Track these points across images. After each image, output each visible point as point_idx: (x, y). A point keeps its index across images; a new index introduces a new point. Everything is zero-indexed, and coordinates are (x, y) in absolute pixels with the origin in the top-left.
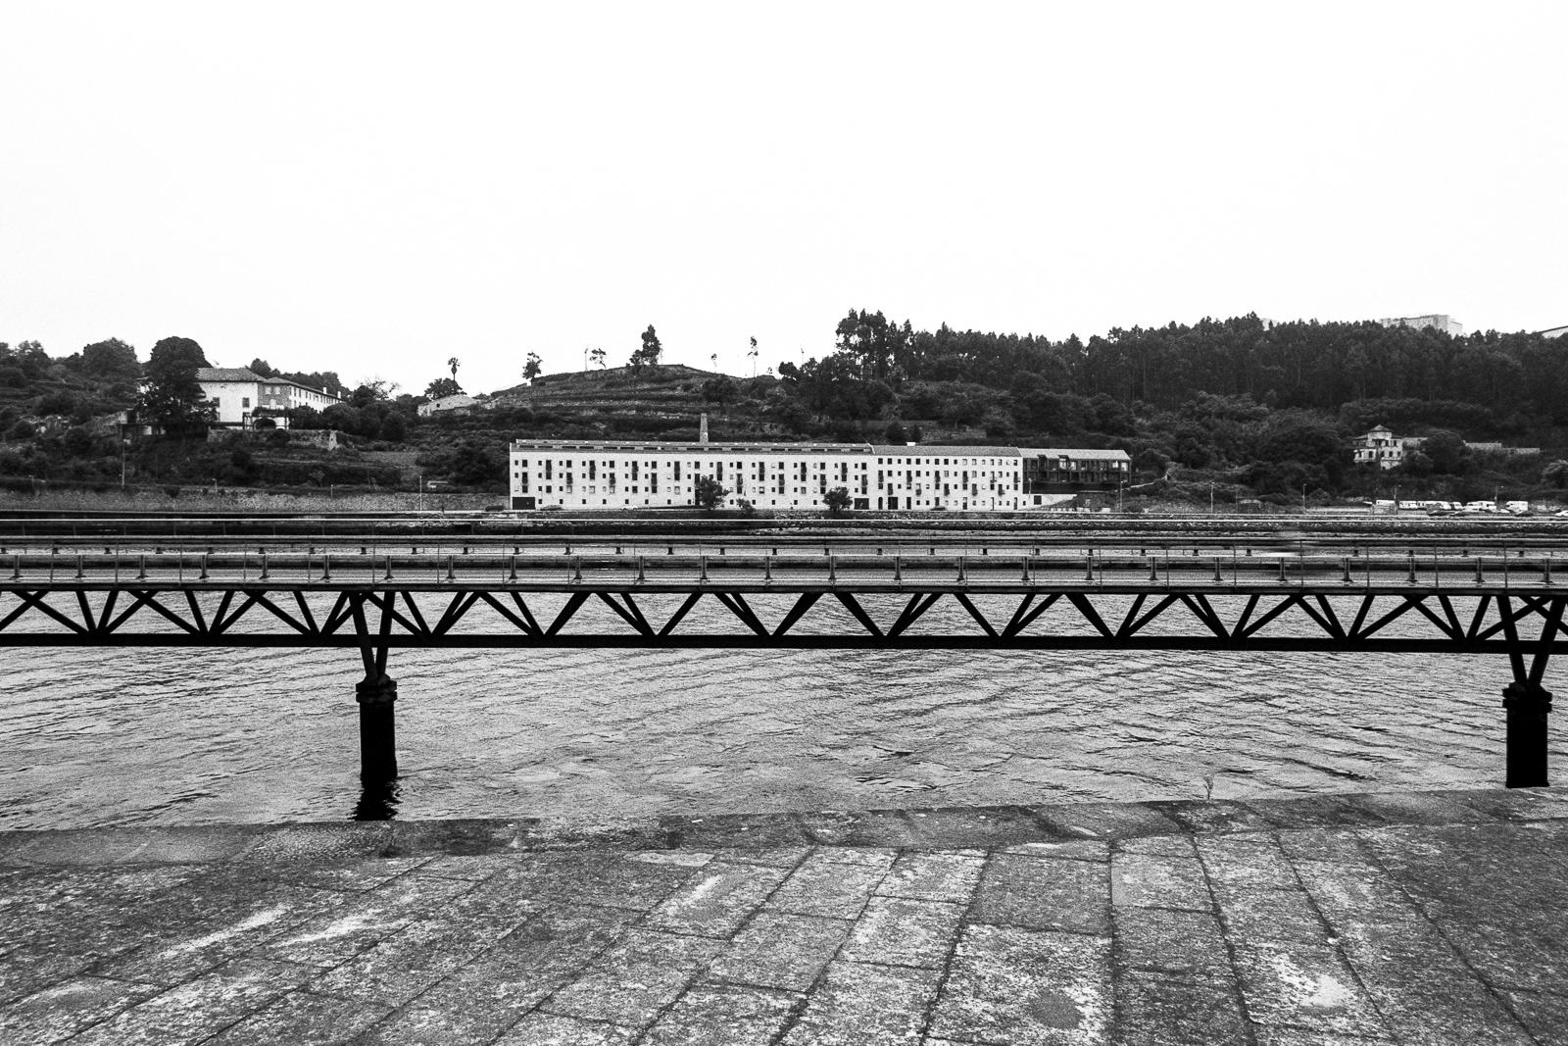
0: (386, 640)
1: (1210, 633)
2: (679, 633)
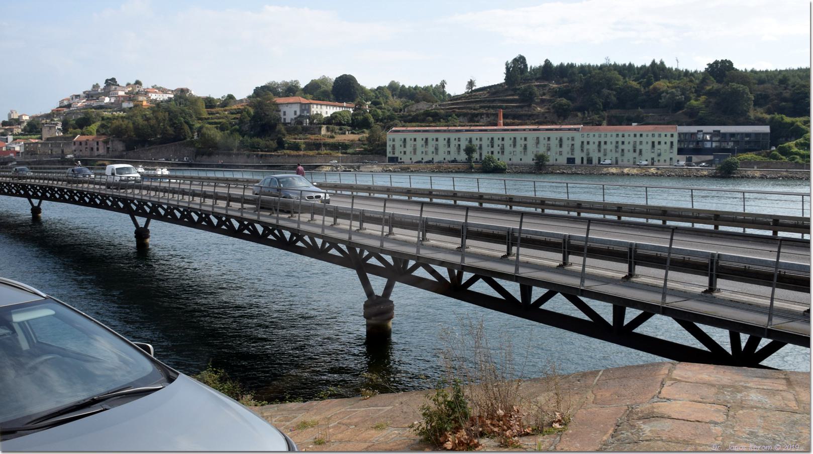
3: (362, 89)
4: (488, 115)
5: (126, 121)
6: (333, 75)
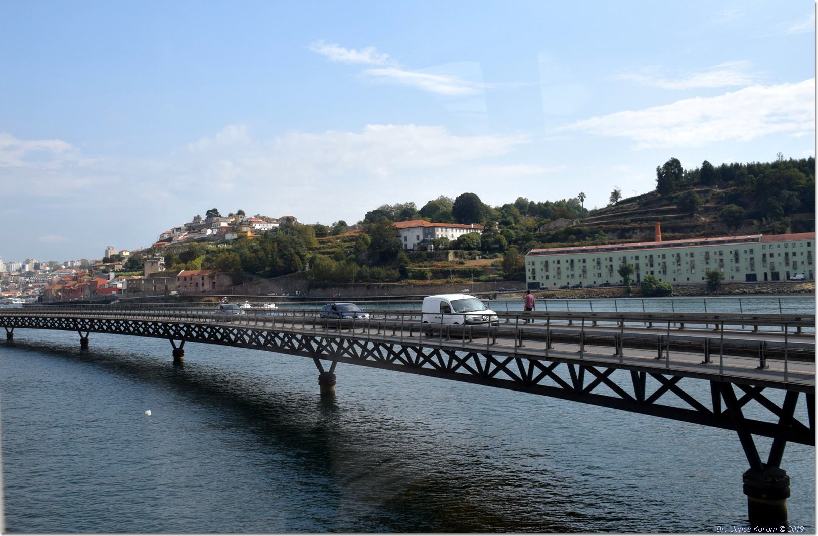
3: (487, 209)
4: (641, 230)
5: (233, 254)
6: (453, 195)
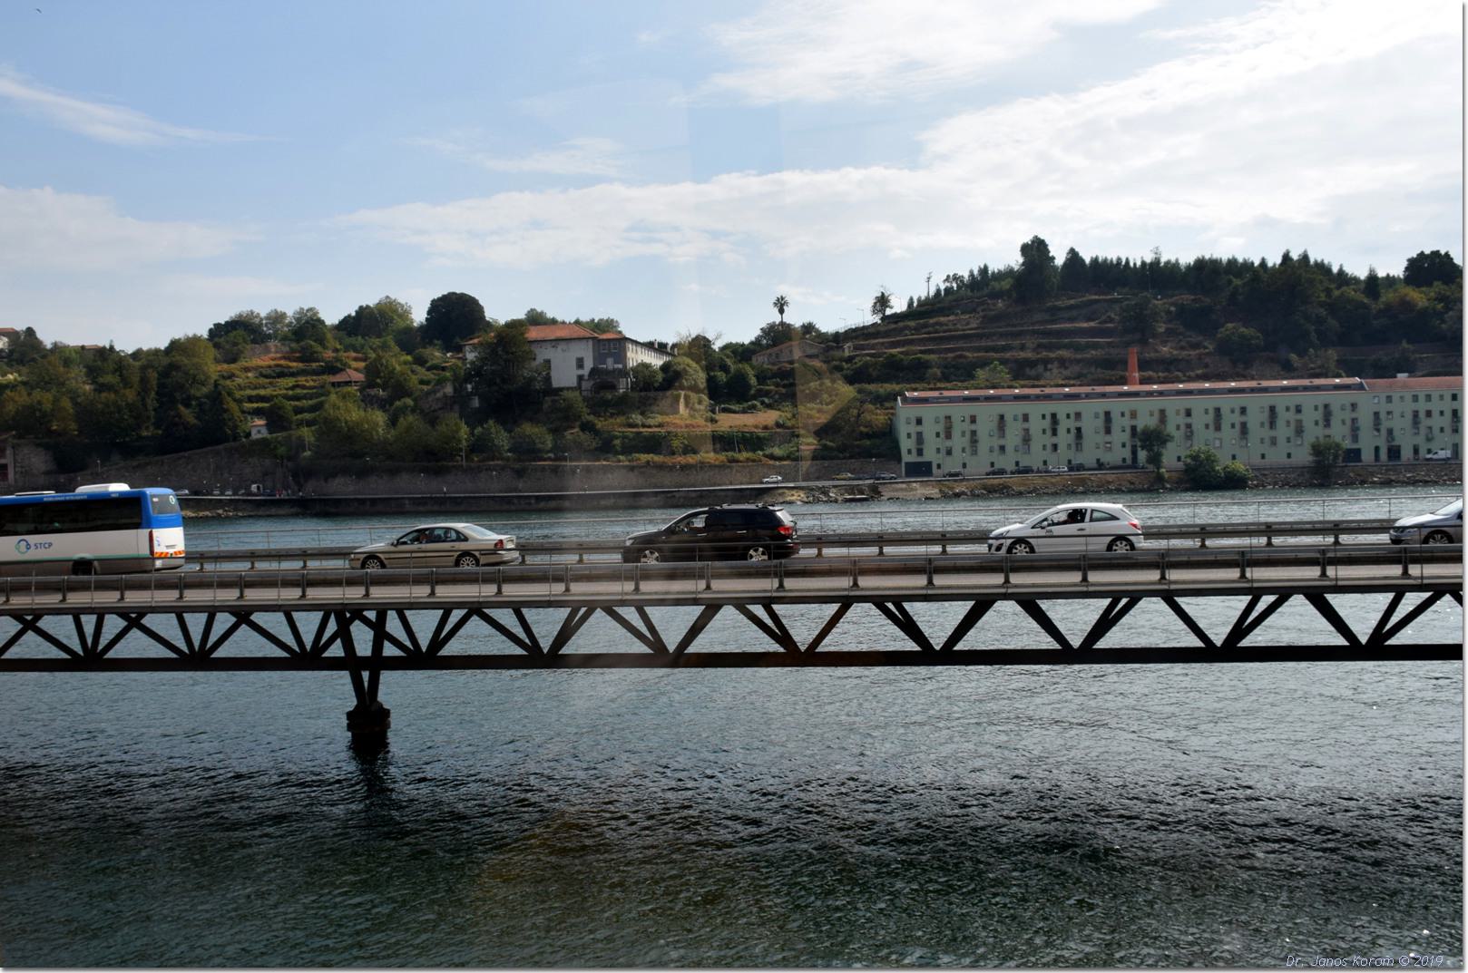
0: (378, 663)
1: (911, 646)
2: (832, 649)
4: (1063, 363)
